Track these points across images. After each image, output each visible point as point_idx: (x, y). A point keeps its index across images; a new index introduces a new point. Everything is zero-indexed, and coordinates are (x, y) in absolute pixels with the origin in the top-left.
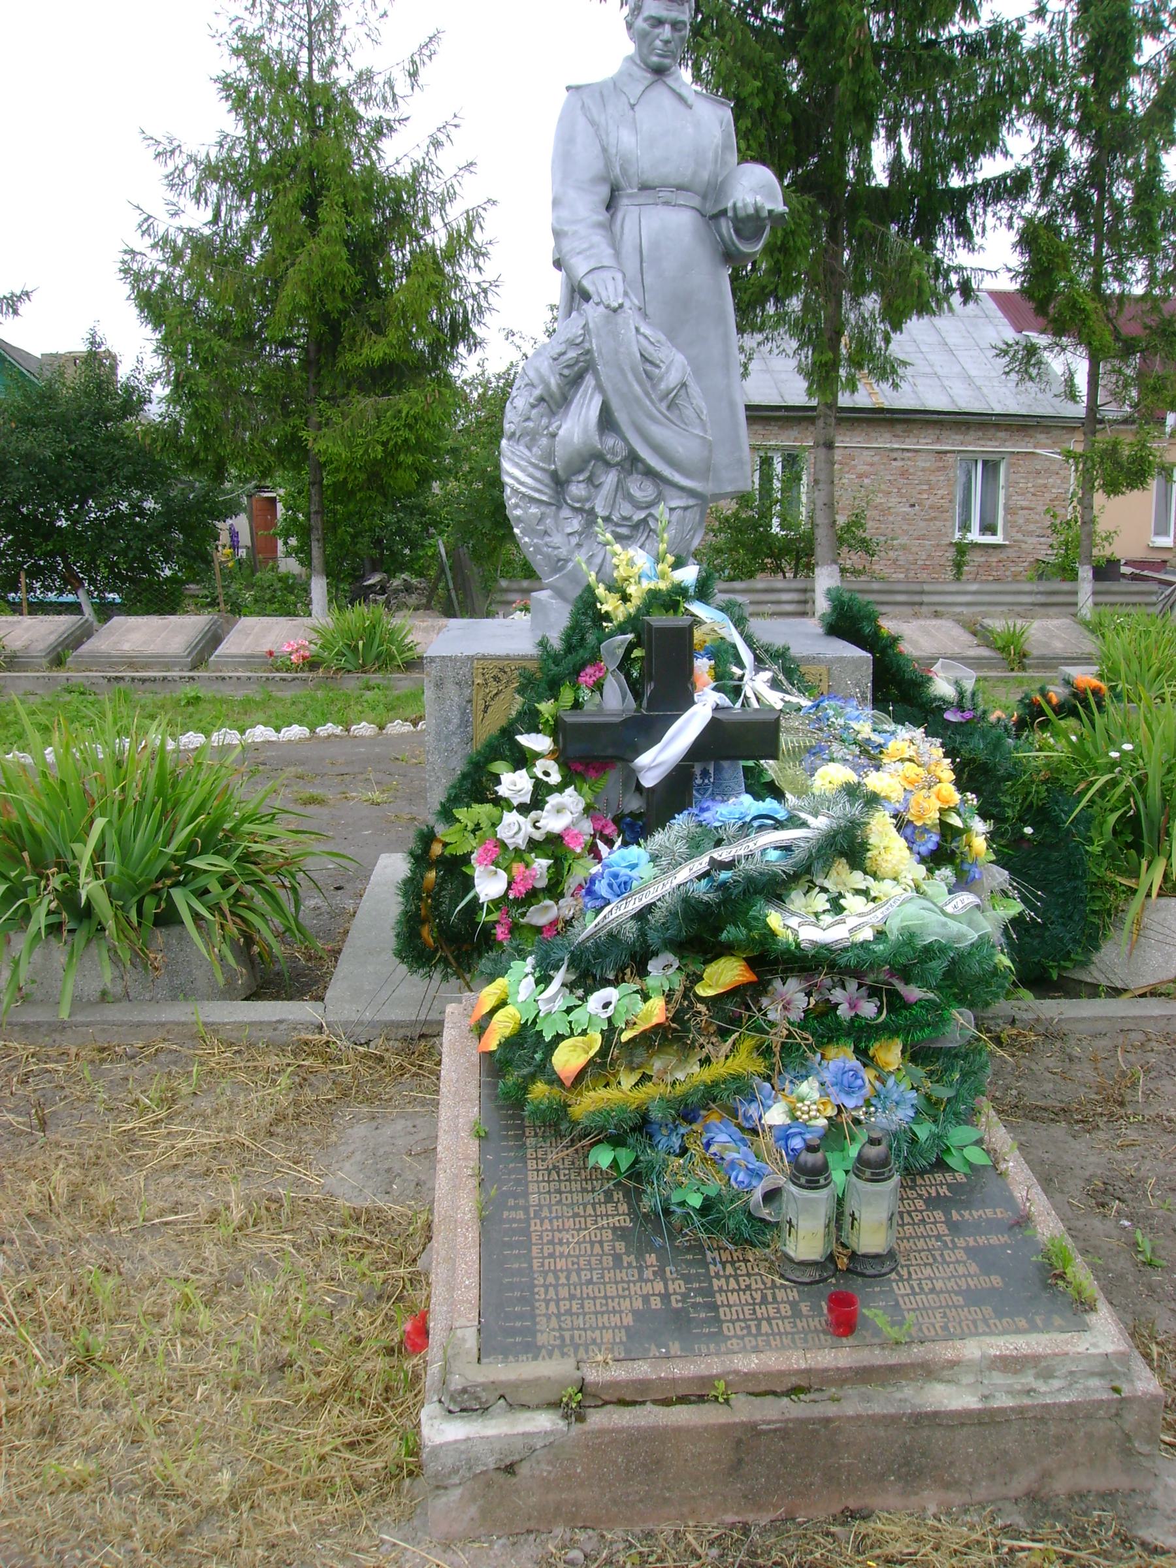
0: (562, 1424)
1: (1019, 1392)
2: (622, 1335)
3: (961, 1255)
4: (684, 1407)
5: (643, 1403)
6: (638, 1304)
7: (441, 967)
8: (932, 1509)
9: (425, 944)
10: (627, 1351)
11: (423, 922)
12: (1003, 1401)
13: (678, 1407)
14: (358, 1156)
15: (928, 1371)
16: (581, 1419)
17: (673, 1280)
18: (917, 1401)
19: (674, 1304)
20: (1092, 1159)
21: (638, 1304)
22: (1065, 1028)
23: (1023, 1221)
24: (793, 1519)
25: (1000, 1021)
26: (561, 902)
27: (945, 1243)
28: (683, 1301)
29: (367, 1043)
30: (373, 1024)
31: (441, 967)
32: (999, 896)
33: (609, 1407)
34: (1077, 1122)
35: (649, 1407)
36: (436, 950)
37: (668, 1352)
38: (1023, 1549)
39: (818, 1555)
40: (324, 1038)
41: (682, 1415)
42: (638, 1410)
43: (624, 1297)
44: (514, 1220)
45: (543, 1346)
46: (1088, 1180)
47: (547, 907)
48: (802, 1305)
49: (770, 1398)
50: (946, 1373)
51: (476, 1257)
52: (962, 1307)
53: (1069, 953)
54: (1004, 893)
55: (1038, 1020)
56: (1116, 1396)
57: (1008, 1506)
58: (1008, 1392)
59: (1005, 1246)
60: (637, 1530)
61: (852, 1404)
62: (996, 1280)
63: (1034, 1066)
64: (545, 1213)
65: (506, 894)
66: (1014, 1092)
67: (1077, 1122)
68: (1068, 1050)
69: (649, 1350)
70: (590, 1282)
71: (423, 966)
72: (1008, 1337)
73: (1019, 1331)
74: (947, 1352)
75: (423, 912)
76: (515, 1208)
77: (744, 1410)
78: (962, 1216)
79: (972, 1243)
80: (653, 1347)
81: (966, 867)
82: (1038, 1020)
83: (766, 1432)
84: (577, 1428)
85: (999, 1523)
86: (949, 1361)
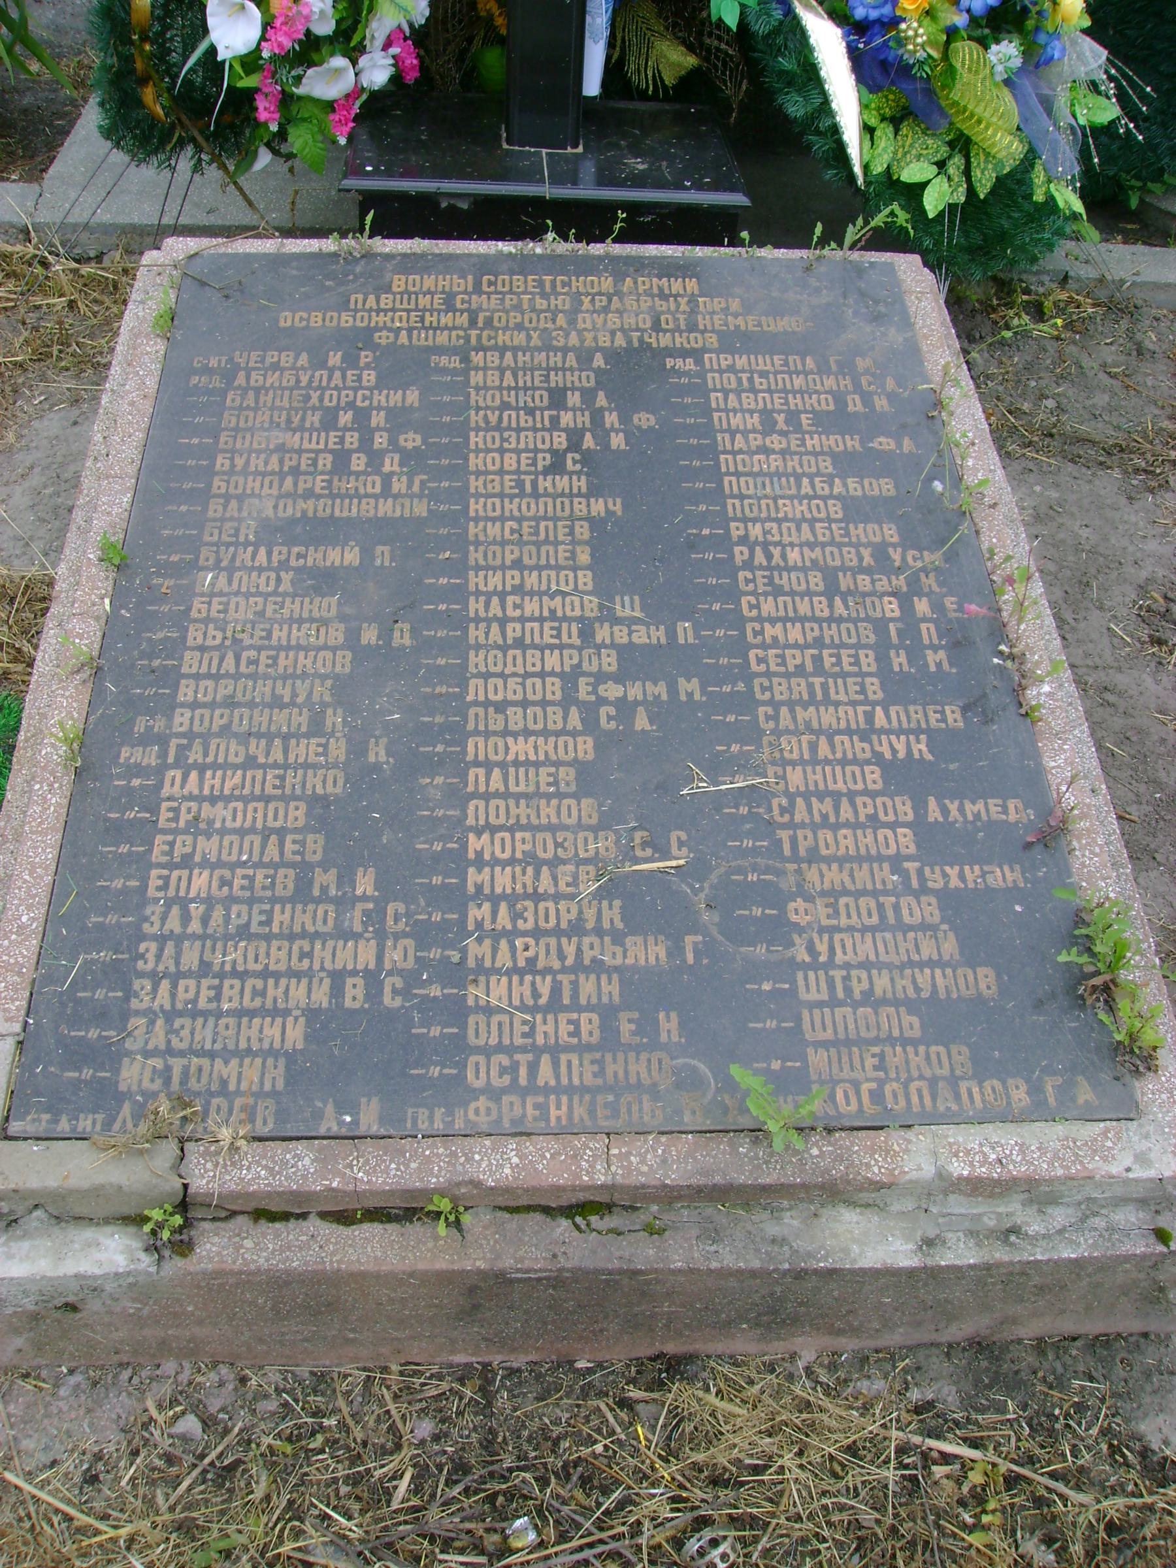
0: (146, 1261)
1: (991, 1233)
2: (276, 1076)
3: (930, 910)
4: (377, 1228)
5: (303, 1216)
6: (321, 996)
7: (190, 150)
8: (807, 1356)
9: (153, 117)
10: (281, 1115)
11: (144, 81)
12: (960, 1253)
13: (366, 1226)
14: (36, 479)
15: (834, 1192)
16: (183, 1247)
17: (397, 937)
18: (801, 1245)
19: (387, 1000)
20: (1152, 546)
21: (321, 996)
22: (1139, 297)
23: (1050, 835)
24: (571, 1362)
25: (1046, 279)
26: (363, 61)
27: (905, 875)
28: (405, 993)
29: (99, 258)
30: (106, 229)
31: (190, 150)
32: (1083, 90)
33: (241, 1220)
34: (1137, 471)
35: (314, 1224)
36: (173, 127)
37: (355, 1122)
38: (946, 1458)
39: (599, 1448)
40: (31, 250)
41: (370, 1248)
42: (291, 1232)
43: (298, 975)
44: (444, 371)
45: (128, 1095)
46: (1143, 589)
47: (339, 71)
48: (624, 1016)
49: (538, 1216)
50: (864, 1196)
51: (51, 855)
52: (915, 1042)
53: (1162, 171)
54: (1094, 86)
55: (1102, 280)
56: (1161, 1248)
57: (937, 1363)
58: (971, 1233)
59: (1012, 893)
60: (304, 1371)
61: (681, 1252)
62: (985, 980)
63: (1086, 362)
64: (195, 755)
65: (258, 48)
66: (1050, 403)
67: (1137, 471)
68: (1139, 336)
69: (318, 1115)
70: (244, 932)
71: (155, 152)
72: (988, 1128)
73: (1008, 1117)
74: (869, 1158)
75: (139, 65)
76: (146, 740)
77: (489, 1247)
78: (945, 811)
79: (955, 882)
80: (330, 1109)
81: (1042, 38)
82: (1102, 280)
83: (519, 1280)
84: (175, 1265)
85: (915, 1395)
86: (871, 1182)
